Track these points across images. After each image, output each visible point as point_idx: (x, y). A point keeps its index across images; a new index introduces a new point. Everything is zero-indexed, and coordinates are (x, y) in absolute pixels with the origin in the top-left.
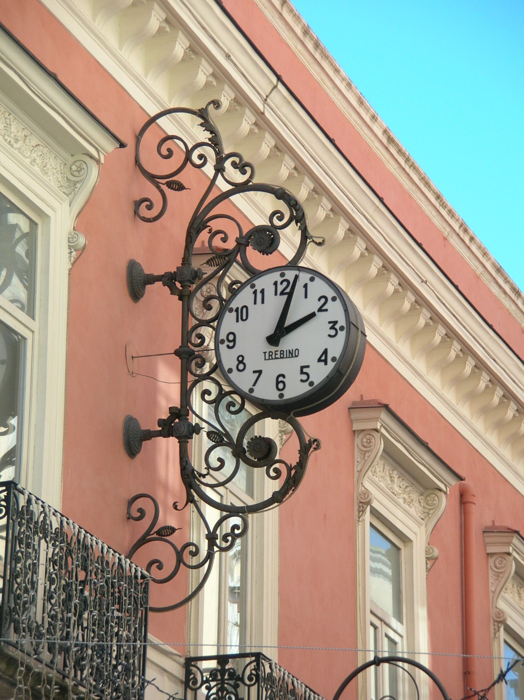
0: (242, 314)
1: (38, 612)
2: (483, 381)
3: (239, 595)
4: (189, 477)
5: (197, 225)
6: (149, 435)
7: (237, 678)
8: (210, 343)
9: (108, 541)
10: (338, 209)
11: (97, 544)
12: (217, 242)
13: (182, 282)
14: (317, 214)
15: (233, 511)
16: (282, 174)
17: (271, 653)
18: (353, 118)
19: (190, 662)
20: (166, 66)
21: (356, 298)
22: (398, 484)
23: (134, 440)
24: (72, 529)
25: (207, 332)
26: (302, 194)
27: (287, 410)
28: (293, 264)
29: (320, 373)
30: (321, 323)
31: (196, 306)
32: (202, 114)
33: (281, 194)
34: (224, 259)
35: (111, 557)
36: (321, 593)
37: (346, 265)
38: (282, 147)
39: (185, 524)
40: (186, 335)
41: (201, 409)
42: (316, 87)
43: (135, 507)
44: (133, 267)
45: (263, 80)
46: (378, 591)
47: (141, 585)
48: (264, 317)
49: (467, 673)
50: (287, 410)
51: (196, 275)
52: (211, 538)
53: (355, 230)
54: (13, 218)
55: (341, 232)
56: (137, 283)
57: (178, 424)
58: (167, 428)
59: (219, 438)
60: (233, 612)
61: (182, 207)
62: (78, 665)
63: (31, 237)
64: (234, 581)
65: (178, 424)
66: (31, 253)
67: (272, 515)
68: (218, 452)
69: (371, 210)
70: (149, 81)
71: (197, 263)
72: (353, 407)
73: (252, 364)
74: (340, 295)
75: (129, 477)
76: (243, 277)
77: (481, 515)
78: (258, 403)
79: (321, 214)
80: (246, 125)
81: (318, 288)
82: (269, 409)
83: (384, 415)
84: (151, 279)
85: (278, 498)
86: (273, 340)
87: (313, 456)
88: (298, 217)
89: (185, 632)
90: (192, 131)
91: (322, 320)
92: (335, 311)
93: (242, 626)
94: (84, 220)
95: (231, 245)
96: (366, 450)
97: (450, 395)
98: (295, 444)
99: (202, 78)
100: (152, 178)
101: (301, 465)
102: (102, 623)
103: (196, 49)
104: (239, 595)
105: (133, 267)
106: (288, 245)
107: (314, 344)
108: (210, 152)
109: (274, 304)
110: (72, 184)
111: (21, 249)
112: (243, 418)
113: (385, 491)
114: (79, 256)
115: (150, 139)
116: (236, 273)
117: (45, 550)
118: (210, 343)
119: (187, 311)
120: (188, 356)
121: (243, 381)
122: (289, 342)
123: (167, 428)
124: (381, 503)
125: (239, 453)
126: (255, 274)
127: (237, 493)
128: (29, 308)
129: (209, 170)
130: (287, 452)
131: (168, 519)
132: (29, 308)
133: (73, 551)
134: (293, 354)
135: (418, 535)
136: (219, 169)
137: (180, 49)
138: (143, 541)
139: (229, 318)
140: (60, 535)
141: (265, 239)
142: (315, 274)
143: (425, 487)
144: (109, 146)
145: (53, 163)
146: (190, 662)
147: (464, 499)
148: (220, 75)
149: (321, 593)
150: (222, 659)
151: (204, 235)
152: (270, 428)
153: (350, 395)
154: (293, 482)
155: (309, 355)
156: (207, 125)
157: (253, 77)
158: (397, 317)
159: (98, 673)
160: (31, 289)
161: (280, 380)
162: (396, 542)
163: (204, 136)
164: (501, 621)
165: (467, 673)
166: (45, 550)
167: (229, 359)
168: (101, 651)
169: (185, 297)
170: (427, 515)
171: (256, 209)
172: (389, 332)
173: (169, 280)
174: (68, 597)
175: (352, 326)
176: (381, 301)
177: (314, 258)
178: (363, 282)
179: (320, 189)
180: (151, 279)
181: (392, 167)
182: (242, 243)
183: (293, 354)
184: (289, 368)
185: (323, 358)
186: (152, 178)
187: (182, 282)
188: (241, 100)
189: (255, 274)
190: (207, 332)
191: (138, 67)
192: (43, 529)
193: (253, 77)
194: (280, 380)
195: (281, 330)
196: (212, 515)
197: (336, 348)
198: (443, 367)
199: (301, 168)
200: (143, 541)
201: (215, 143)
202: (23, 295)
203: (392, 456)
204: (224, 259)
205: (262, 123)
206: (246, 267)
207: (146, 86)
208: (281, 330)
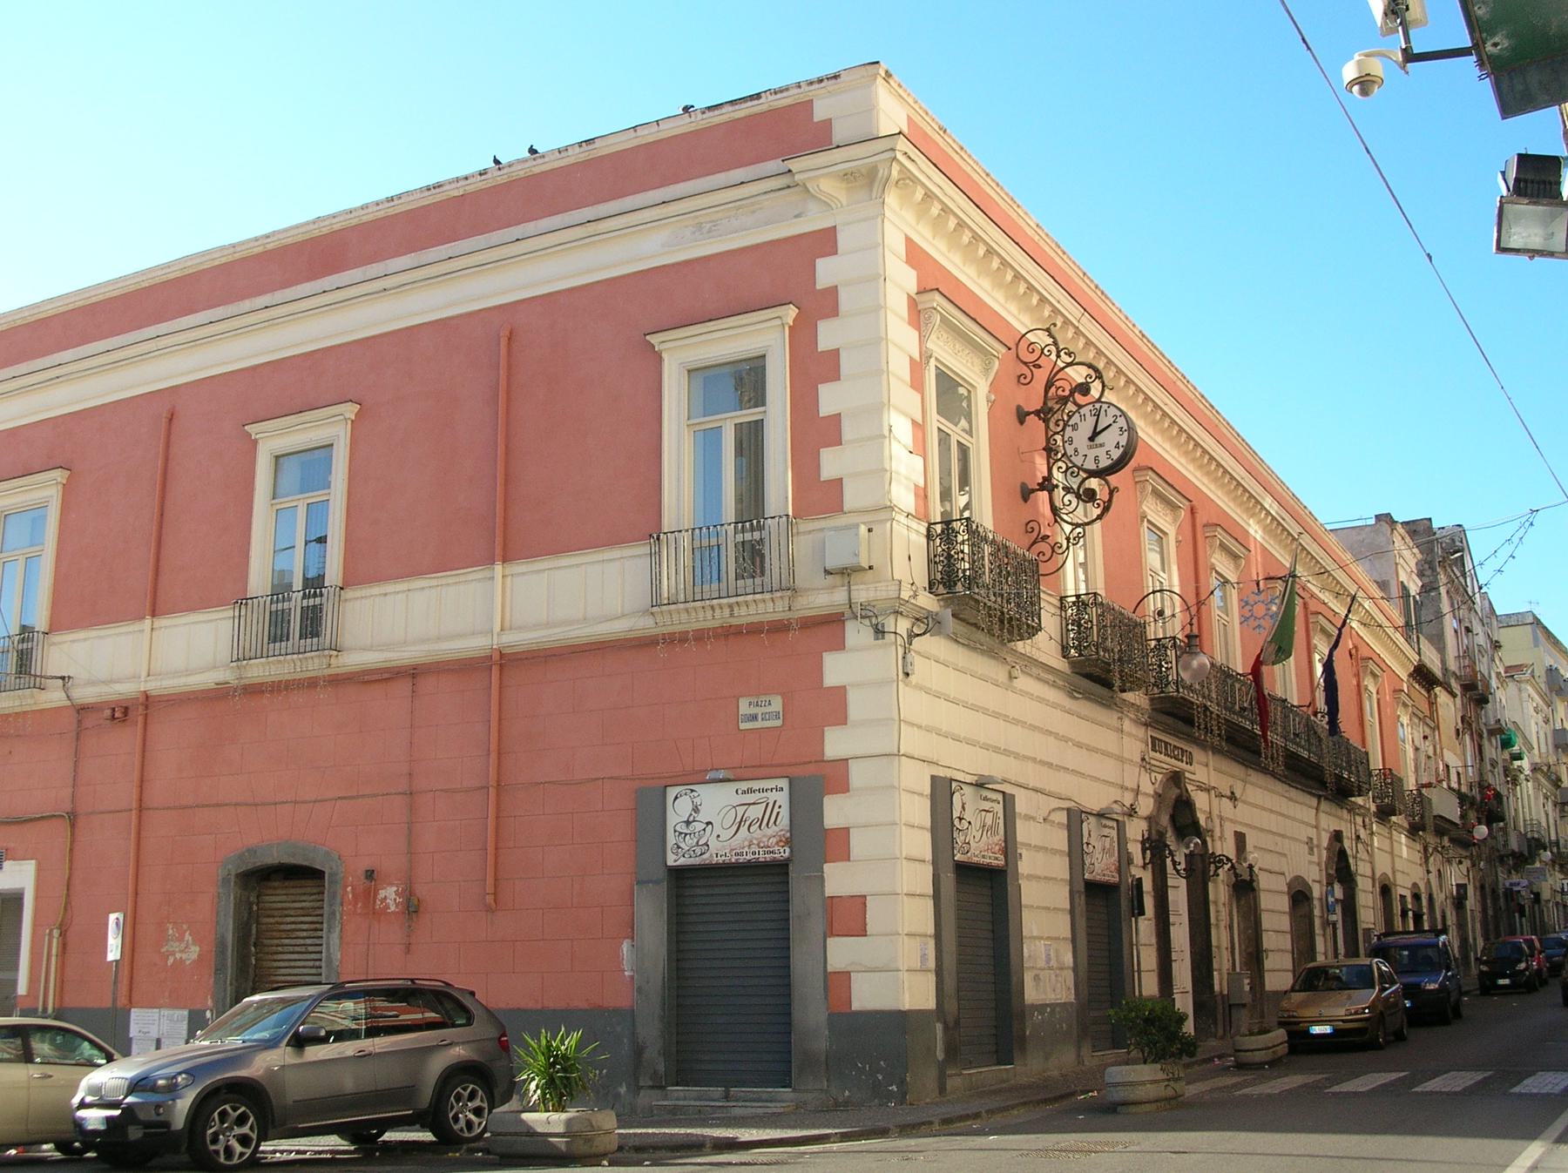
0: (1075, 427)
1: (987, 578)
2: (1240, 491)
3: (1084, 565)
4: (1055, 511)
5: (1049, 384)
6: (1033, 491)
7: (1085, 605)
8: (1060, 443)
9: (1017, 545)
10: (1119, 371)
11: (1012, 545)
12: (1060, 392)
13: (1044, 413)
14: (1109, 375)
15: (1078, 525)
16: (1090, 356)
17: (1101, 592)
18: (1053, 255)
19: (1062, 599)
20: (1029, 309)
21: (1132, 415)
22: (1160, 507)
23: (1026, 494)
24: (999, 539)
25: (1058, 437)
26: (1101, 366)
27: (1101, 473)
28: (1099, 401)
29: (1116, 454)
30: (1115, 428)
31: (1052, 425)
32: (1048, 330)
33: (1090, 366)
34: (1064, 401)
35: (1019, 551)
36: (1124, 562)
37: (1127, 399)
38: (1089, 343)
39: (1054, 534)
40: (1048, 440)
41: (1058, 476)
42: (1104, 314)
43: (1030, 526)
44: (1019, 408)
45: (1077, 311)
46: (1153, 559)
47: (1035, 564)
48: (1086, 428)
49: (1197, 594)
50: (1101, 473)
51: (1051, 409)
52: (1068, 539)
53: (1129, 381)
54: (961, 390)
55: (1122, 383)
56: (1022, 416)
57: (1047, 485)
58: (1042, 487)
59: (1068, 490)
60: (1081, 571)
61: (1041, 376)
62: (1008, 602)
63: (969, 398)
64: (1081, 559)
65: (1047, 485)
66: (969, 406)
67: (1097, 525)
68: (1069, 497)
69: (1064, 301)
70: (951, 255)
71: (1050, 404)
72: (1135, 470)
73: (1082, 452)
74: (1123, 414)
75: (1025, 513)
76: (1074, 408)
77: (1201, 519)
78: (1085, 471)
79: (1111, 374)
80: (1070, 334)
81: (1112, 411)
82: (1092, 474)
83: (937, 296)
84: (1029, 414)
85: (1099, 517)
86: (1091, 439)
87: (1115, 495)
88: (1100, 376)
89: (1058, 585)
90: (1042, 339)
91: (1115, 427)
92: (1122, 422)
93: (1086, 581)
94: (993, 387)
95: (1067, 393)
96: (1143, 490)
97: (1198, 474)
98: (1107, 490)
99: (1047, 313)
100: (1025, 363)
101: (1110, 500)
102: (1017, 582)
103: (1043, 299)
104: (1084, 565)
105: (1019, 408)
106: (1095, 391)
107: (1112, 441)
108: (1053, 349)
109: (1091, 421)
110: (986, 370)
111: (964, 404)
112: (1079, 479)
113: (1155, 512)
114: (992, 405)
115: (1023, 345)
116: (1070, 407)
117: (987, 549)
118: (1060, 443)
119: (1047, 427)
120: (1049, 450)
121: (1078, 461)
122: (1099, 440)
123: (1042, 487)
124: (1152, 516)
125: (1078, 497)
126: (1080, 407)
127: (1079, 516)
128: (970, 433)
129: (1053, 357)
130: (1102, 494)
131: (1046, 531)
132: (970, 433)
133: (1000, 549)
134: (1101, 445)
135: (1171, 530)
136: (1058, 356)
137: (1035, 301)
138: (1034, 543)
139: (1069, 429)
140: (993, 542)
141: (1084, 389)
142: (1110, 404)
143: (1174, 507)
144: (1004, 350)
145: (977, 361)
146: (1062, 599)
147: (1193, 511)
148: (1055, 311)
149: (1124, 562)
150: (1078, 596)
151: (1053, 389)
152: (1094, 483)
153: (1132, 464)
154: (1106, 509)
155: (1110, 446)
156: (1050, 335)
157: (1071, 310)
158: (1154, 423)
159: (1018, 605)
160: (970, 423)
161: (1096, 459)
162: (1161, 535)
163: (1050, 341)
164: (1213, 568)
165: (1197, 594)
166: (987, 549)
167: (1070, 451)
168: (1019, 595)
169: (1046, 421)
170: (1175, 520)
171: (1078, 375)
172: (1150, 431)
173: (1037, 413)
174: (1001, 572)
175: (1131, 429)
176: (1145, 416)
177: (1109, 396)
178: (1136, 407)
179: (1110, 362)
180: (1029, 414)
181: (1145, 349)
182: (1072, 393)
183: (1101, 445)
184: (1101, 452)
185: (1117, 446)
186: (1025, 363)
187: (1044, 413)
188: (1067, 322)
189: (1080, 407)
190: (1058, 437)
191: (1002, 300)
192: (985, 539)
193: (1071, 310)
194: (1096, 459)
195: (1095, 434)
196: (1068, 528)
197: (1123, 441)
198: (1178, 446)
199: (1099, 352)
200: (1034, 543)
201: (1055, 343)
202: (966, 426)
203: (1155, 492)
204: (1064, 401)
205: (1078, 332)
206: (1075, 403)
207: (1020, 320)
208: (1095, 434)
